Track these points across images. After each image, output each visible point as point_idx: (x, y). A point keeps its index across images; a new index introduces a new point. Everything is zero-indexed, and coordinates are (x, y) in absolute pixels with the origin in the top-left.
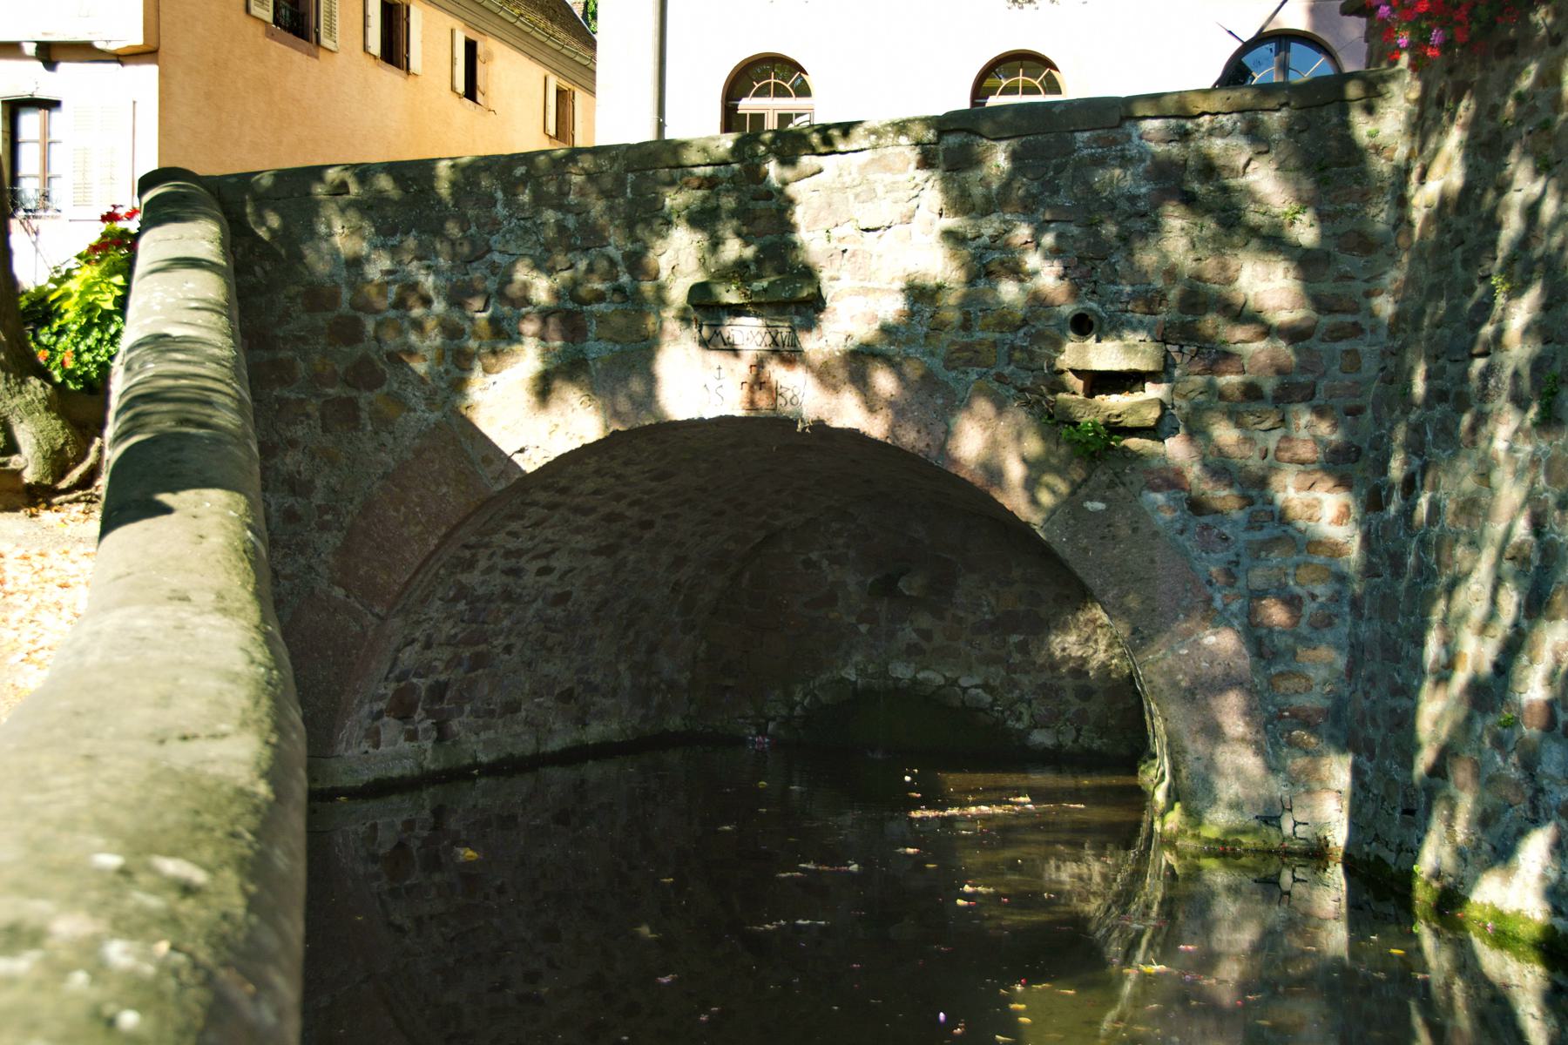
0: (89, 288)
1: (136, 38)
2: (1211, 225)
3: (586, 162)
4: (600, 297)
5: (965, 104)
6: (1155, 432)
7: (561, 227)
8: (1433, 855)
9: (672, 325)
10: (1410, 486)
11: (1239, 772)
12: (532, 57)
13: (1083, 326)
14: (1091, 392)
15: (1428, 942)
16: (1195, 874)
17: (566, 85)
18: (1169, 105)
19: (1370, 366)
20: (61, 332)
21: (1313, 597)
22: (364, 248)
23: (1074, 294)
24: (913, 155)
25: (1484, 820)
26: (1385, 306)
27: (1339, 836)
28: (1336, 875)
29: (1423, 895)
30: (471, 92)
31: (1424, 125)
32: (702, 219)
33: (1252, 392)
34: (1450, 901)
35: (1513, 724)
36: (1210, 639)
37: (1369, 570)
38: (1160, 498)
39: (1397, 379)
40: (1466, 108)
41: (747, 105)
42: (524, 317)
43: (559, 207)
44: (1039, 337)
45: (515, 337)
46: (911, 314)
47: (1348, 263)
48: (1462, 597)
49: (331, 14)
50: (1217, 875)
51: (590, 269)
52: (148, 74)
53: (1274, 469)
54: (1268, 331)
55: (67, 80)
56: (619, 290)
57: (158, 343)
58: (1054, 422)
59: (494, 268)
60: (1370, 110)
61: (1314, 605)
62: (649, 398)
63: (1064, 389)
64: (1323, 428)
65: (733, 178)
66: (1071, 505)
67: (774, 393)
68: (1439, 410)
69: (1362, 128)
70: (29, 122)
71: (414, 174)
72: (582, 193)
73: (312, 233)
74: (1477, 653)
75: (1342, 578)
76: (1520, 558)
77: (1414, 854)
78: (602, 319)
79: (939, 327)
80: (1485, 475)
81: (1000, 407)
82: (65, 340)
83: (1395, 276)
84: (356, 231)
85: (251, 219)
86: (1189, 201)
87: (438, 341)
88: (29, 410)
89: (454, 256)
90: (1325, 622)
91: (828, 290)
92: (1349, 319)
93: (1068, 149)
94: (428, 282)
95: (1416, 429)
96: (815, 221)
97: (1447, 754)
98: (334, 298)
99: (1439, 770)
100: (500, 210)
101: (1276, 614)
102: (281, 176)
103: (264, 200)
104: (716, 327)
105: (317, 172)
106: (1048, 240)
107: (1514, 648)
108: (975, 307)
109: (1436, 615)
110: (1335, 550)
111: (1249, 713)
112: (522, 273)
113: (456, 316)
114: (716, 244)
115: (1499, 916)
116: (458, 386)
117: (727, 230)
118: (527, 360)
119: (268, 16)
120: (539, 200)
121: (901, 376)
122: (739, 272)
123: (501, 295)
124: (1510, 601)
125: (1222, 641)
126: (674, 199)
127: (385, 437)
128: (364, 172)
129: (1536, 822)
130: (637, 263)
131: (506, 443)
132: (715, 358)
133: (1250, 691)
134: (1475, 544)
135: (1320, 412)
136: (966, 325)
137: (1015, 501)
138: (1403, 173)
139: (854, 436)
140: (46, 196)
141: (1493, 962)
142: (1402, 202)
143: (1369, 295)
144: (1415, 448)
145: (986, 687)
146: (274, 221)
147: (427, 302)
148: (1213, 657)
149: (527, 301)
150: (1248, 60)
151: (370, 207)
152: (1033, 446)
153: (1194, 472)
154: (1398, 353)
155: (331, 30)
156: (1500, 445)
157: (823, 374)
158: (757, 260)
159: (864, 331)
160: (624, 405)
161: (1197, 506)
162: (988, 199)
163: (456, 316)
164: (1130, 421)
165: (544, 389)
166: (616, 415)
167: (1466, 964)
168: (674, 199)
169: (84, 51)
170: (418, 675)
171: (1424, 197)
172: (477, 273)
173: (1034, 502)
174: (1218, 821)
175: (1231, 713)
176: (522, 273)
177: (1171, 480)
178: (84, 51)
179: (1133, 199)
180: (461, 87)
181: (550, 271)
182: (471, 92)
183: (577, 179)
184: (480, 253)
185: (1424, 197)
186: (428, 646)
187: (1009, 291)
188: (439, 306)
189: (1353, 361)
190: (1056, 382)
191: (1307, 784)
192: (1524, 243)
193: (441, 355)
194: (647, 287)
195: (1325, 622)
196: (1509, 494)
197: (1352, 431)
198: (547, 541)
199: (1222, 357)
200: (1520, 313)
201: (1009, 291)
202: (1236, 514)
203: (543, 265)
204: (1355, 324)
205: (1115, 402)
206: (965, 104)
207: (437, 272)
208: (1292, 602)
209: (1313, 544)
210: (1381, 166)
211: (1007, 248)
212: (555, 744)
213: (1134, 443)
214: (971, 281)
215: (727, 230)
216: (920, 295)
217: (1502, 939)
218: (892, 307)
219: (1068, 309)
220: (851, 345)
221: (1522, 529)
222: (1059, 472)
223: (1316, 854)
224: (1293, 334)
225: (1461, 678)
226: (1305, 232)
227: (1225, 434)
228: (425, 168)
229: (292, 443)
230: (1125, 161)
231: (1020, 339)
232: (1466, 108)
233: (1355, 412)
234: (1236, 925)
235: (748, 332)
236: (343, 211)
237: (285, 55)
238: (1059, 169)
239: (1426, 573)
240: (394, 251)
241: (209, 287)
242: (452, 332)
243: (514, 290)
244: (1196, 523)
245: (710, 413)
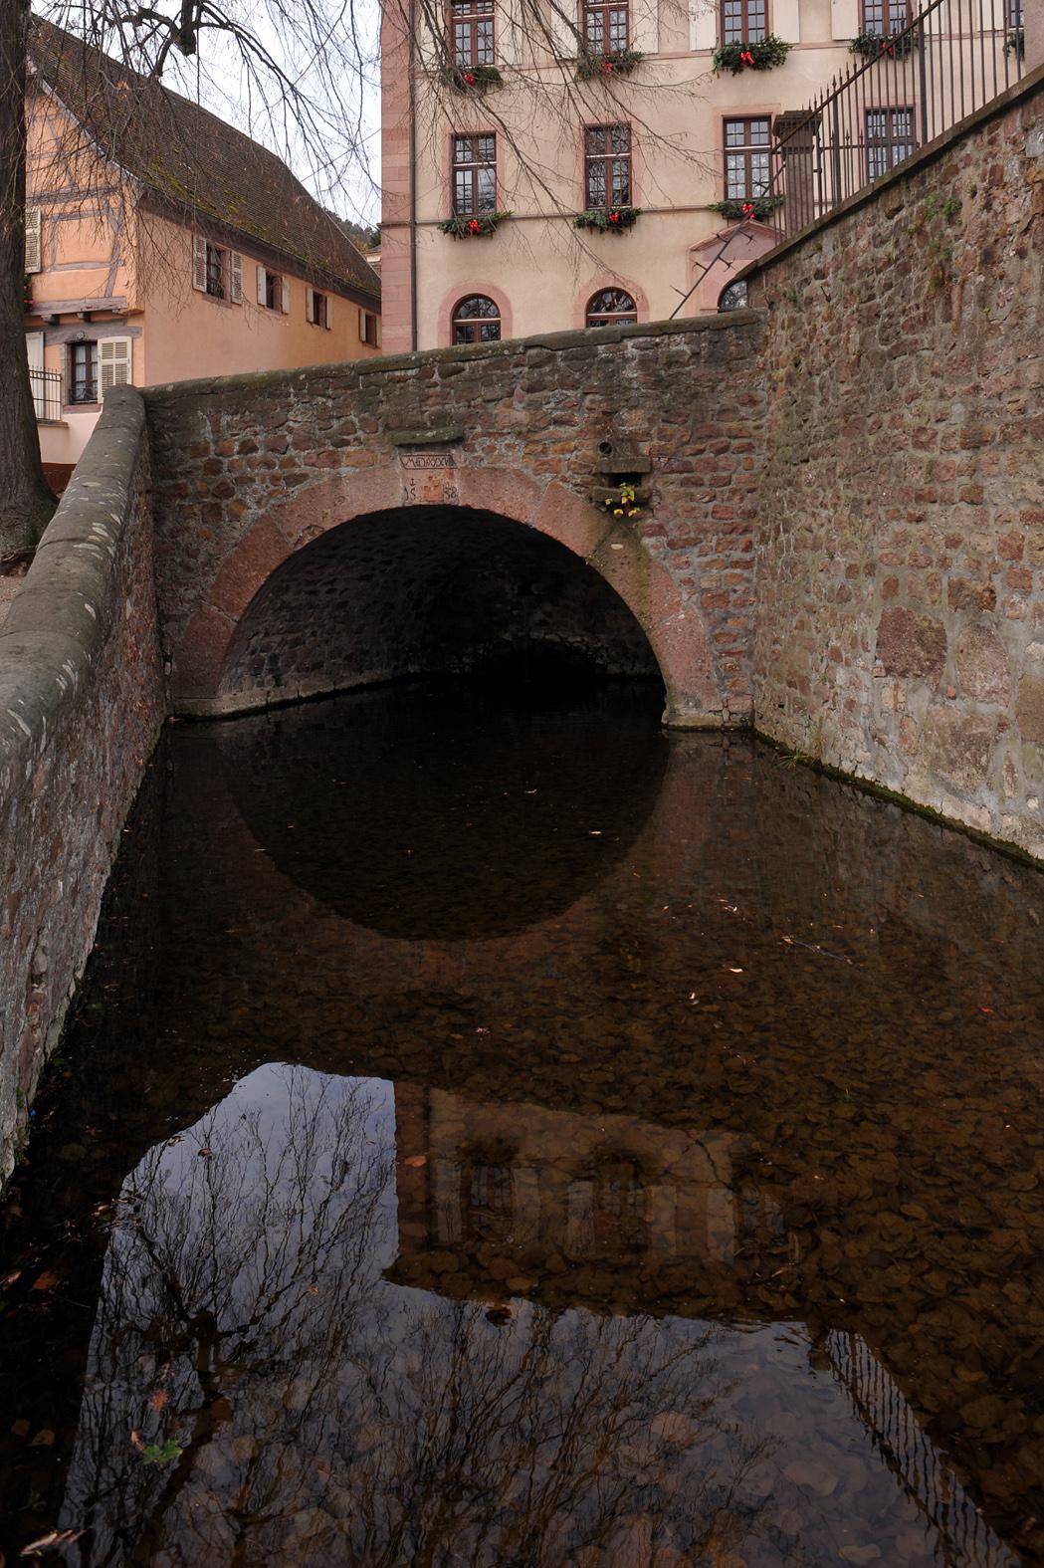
12: (351, 300)
17: (371, 313)
21: (735, 591)
61: (736, 596)
70: (81, 357)
92: (746, 441)
98: (206, 450)
119: (204, 289)
127: (237, 525)
170: (262, 651)
198: (330, 575)
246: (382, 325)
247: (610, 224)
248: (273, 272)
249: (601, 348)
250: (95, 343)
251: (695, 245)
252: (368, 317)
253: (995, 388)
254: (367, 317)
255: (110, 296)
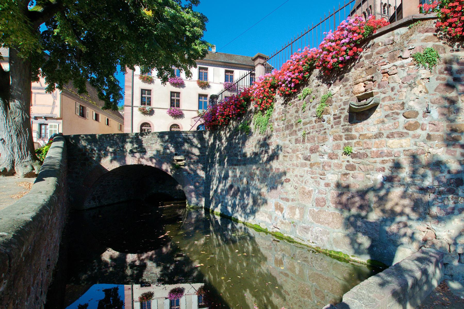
0: (47, 149)
1: (59, 117)
2: (189, 145)
3: (116, 135)
4: (118, 151)
5: (169, 130)
6: (184, 166)
7: (113, 143)
8: (211, 207)
9: (128, 154)
10: (209, 171)
11: (194, 200)
13: (176, 155)
14: (177, 162)
15: (211, 215)
16: (190, 210)
18: (185, 132)
19: (206, 159)
20: (43, 154)
22: (86, 145)
23: (175, 151)
24: (157, 136)
25: (216, 203)
26: (207, 153)
27: (204, 206)
28: (203, 209)
29: (210, 211)
30: (108, 124)
31: (210, 136)
32: (131, 142)
33: (194, 161)
34: (213, 211)
35: (218, 194)
36: (190, 187)
37: (206, 179)
38: (185, 173)
39: (208, 160)
40: (213, 135)
41: (143, 128)
42: (108, 153)
43: (113, 140)
44: (171, 156)
45: (107, 155)
46: (157, 153)
47: (203, 149)
48: (213, 182)
49: (88, 115)
50: (192, 210)
51: (117, 148)
52: (61, 121)
53: (197, 169)
54: (195, 155)
55: (49, 122)
56: (121, 150)
57: (50, 158)
58: (173, 165)
59: (104, 147)
60: (205, 134)
62: (125, 162)
63: (174, 161)
64: (201, 165)
65: (135, 138)
66: (175, 174)
67: (141, 162)
68: (211, 164)
69: (204, 136)
70: (43, 127)
71: (93, 136)
72: (116, 139)
73: (79, 143)
74: (215, 187)
75: (203, 180)
76: (218, 178)
77: (210, 207)
78: (119, 153)
79: (160, 155)
80: (215, 170)
81: (167, 163)
82: (43, 155)
83: (208, 150)
84: (85, 142)
85: (70, 141)
86: (188, 143)
87: (97, 155)
88: (36, 165)
89: (99, 146)
90: (202, 184)
91: (147, 150)
93: (174, 136)
94: (95, 149)
95: (210, 165)
96: (145, 143)
97: (212, 197)
99: (212, 199)
100: (105, 140)
101: (197, 184)
102: (75, 136)
103: (72, 139)
104: (133, 154)
105: (80, 135)
106: (172, 146)
107: (218, 187)
108: (164, 153)
109: (211, 184)
110: (203, 178)
111: (195, 194)
112: (108, 148)
113: (99, 153)
114: (133, 145)
115: (217, 212)
116: (100, 161)
117: (135, 143)
118: (109, 158)
119: (79, 115)
120: (110, 140)
121: (156, 160)
122: (136, 148)
123: (105, 150)
124: (217, 182)
125: (192, 187)
126: (128, 140)
128: (86, 135)
129: (219, 203)
130: (123, 147)
131: (106, 168)
132: (133, 158)
133: (195, 192)
134: (215, 177)
135: (201, 164)
136: (163, 154)
137: (169, 173)
138: (208, 140)
139: (150, 166)
140: (45, 136)
141: (216, 217)
142: (208, 143)
143: (206, 152)
144: (209, 167)
145: (169, 192)
146: (74, 141)
147: (95, 151)
148: (191, 189)
149: (109, 151)
150: (200, 126)
151: (87, 140)
152: (171, 167)
153: (188, 170)
154: (208, 158)
155: (88, 117)
156: (216, 167)
157: (147, 160)
158: (138, 147)
159: (152, 155)
160: (122, 163)
161: (189, 173)
162: (165, 141)
163: (99, 153)
164: (181, 165)
165: (111, 161)
166: (121, 164)
167: (214, 217)
168: (128, 140)
169: (51, 118)
171: (210, 143)
172: (102, 147)
173: (171, 173)
174: (192, 205)
175: (193, 194)
176: (108, 148)
177: (186, 170)
178: (51, 118)
179: (181, 142)
180: (106, 124)
181: (112, 148)
182: (108, 124)
183: (115, 137)
184: (102, 145)
185: (210, 143)
186: (97, 191)
187: (168, 151)
188: (97, 152)
189: (204, 159)
190: (173, 160)
191: (201, 201)
192: (218, 148)
193: (97, 158)
194: (125, 150)
195: (202, 184)
196: (217, 172)
197: (204, 165)
199: (191, 158)
200: (218, 154)
201: (168, 151)
202: (193, 174)
203: (111, 147)
204: (416, 122)
205: (180, 163)
206: (169, 130)
207: (97, 147)
208: (199, 183)
209: (200, 177)
210: (206, 140)
211: (168, 146)
212: (115, 202)
213: (182, 167)
214: (164, 150)
215: (135, 143)
216: (158, 151)
217: (217, 214)
218: (155, 153)
219: (174, 153)
220: (150, 156)
221: (218, 175)
222: (174, 170)
223: (202, 208)
224: (198, 156)
225: (214, 190)
226: (199, 146)
227: (192, 166)
228: (95, 135)
229: (77, 168)
230: (180, 138)
231: (169, 156)
232: (213, 135)
233: (204, 164)
234: (194, 215)
235: (138, 155)
236: (83, 140)
237: (81, 119)
238: (173, 138)
239: (211, 180)
240: (91, 145)
241: (60, 150)
242: (99, 154)
243: (107, 150)
244: (189, 175)
245: (132, 164)
246: (124, 127)
247: (448, 214)
248: (97, 113)
249: (175, 135)
250: (47, 124)
251: (192, 117)
252: (120, 125)
253: (249, 147)
254: (120, 125)
255: (52, 114)
